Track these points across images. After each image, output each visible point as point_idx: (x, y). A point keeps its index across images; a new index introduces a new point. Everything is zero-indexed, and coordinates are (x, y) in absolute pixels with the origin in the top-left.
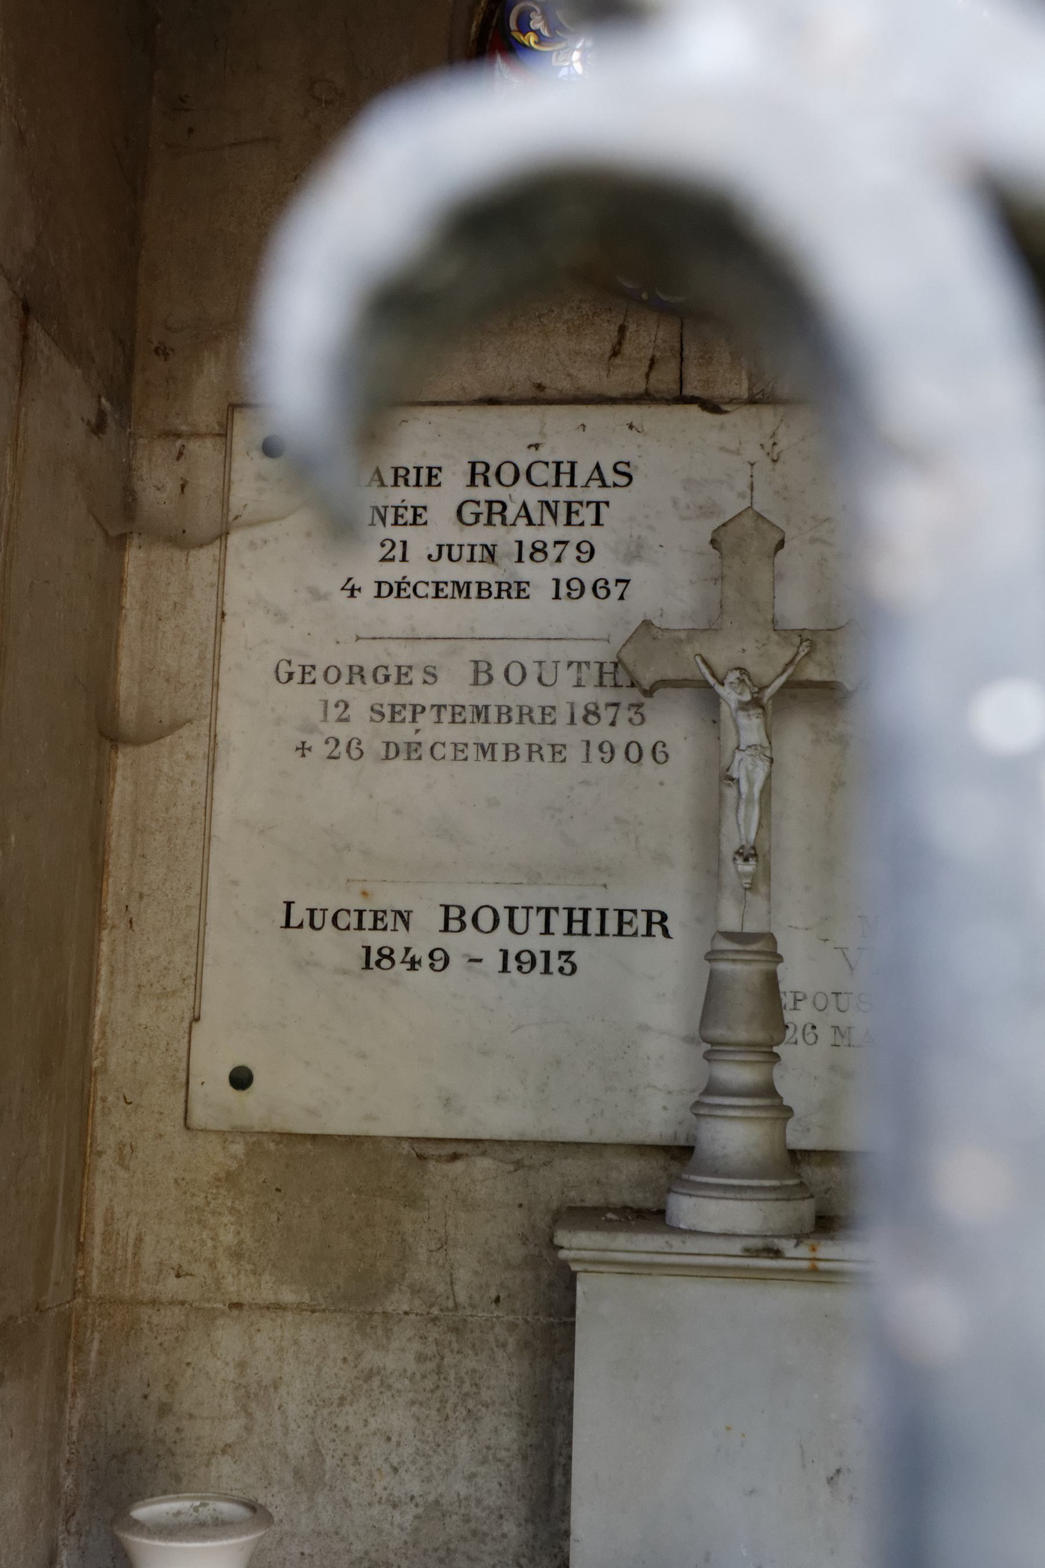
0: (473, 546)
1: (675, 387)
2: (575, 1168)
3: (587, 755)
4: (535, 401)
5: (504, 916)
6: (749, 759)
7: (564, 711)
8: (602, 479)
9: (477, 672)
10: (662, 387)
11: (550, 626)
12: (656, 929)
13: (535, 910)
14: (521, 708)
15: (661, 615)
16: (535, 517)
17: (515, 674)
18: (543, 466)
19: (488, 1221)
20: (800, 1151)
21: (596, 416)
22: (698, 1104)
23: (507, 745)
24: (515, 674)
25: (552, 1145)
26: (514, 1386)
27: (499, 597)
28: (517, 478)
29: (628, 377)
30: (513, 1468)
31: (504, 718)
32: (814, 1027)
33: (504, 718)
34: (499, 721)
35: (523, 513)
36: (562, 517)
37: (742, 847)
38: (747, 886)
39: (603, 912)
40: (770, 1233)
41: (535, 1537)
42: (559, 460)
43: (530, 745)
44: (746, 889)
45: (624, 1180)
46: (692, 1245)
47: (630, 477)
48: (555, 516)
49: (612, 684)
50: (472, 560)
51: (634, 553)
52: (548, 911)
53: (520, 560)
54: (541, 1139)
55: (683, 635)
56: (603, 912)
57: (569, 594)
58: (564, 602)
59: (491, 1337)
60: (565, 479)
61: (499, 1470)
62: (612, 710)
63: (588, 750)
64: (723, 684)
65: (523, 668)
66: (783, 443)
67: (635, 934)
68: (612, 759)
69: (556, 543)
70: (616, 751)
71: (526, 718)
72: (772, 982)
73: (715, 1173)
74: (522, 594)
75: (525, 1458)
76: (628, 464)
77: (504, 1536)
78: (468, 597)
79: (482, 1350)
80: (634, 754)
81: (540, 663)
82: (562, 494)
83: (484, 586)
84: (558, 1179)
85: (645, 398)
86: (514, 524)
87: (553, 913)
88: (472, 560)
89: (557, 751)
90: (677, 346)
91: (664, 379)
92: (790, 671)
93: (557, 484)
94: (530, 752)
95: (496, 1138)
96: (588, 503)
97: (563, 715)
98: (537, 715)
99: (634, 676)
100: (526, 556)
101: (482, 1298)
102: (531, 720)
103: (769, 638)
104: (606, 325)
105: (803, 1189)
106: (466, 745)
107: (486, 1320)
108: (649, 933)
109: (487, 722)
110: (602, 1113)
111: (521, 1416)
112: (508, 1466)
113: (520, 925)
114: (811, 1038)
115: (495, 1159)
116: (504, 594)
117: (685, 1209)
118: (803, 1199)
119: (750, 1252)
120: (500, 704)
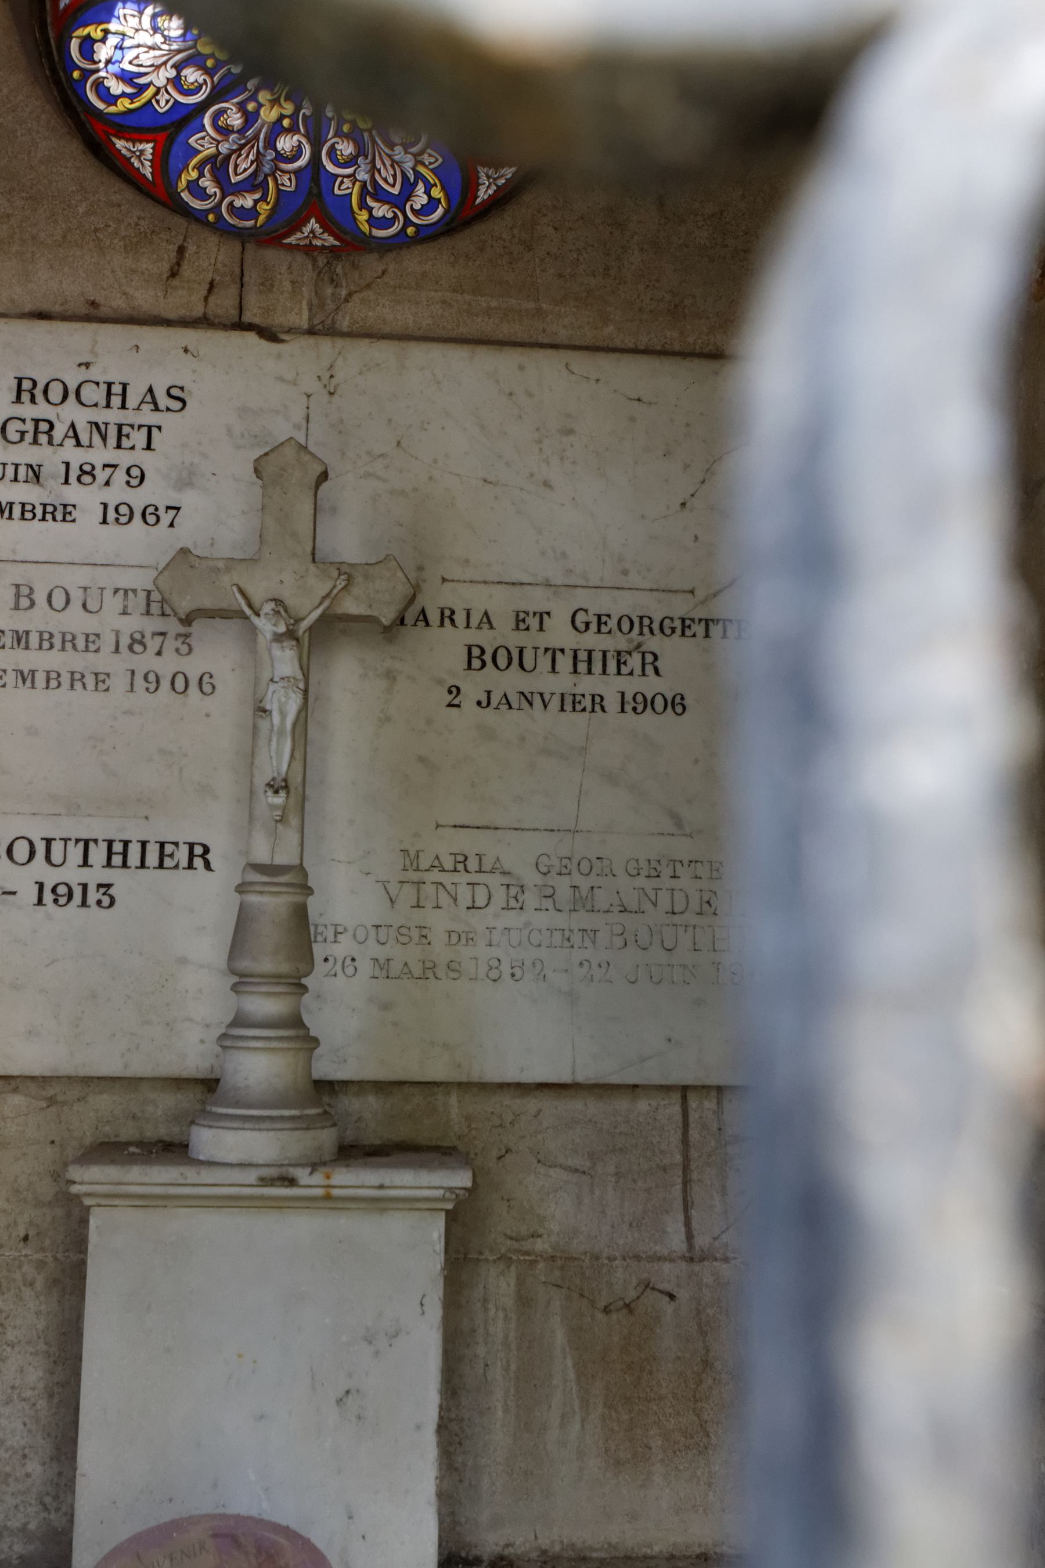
0: (17, 466)
1: (235, 313)
2: (104, 1102)
3: (132, 684)
4: (87, 319)
5: (40, 848)
6: (282, 690)
7: (108, 639)
8: (155, 403)
9: (18, 596)
10: (220, 312)
11: (94, 551)
12: (198, 862)
13: (73, 841)
14: (64, 634)
15: (212, 544)
16: (84, 438)
17: (59, 600)
18: (94, 386)
19: (17, 1159)
20: (338, 1082)
21: (151, 337)
22: (224, 1036)
23: (48, 672)
24: (59, 600)
25: (87, 1081)
26: (41, 1324)
27: (44, 519)
28: (65, 397)
29: (186, 299)
30: (38, 1407)
31: (46, 645)
32: (353, 960)
33: (46, 645)
34: (40, 648)
35: (71, 433)
36: (112, 441)
37: (274, 779)
38: (278, 818)
39: (144, 844)
40: (287, 1162)
41: (60, 1474)
42: (110, 380)
43: (72, 673)
44: (277, 821)
45: (158, 1113)
46: (207, 1175)
47: (184, 402)
48: (104, 439)
49: (160, 613)
50: (16, 480)
51: (186, 480)
52: (87, 843)
53: (66, 482)
54: (73, 1074)
55: (221, 564)
56: (144, 844)
57: (117, 520)
58: (112, 528)
59: (18, 1276)
60: (116, 401)
61: (23, 1409)
62: (159, 639)
63: (132, 679)
64: (258, 615)
65: (67, 594)
66: (340, 376)
67: (176, 867)
68: (157, 689)
69: (105, 466)
70: (162, 681)
71: (69, 645)
72: (300, 915)
73: (237, 1104)
74: (68, 518)
75: (51, 1396)
76: (182, 388)
77: (28, 1475)
78: (10, 518)
79: (9, 1290)
80: (181, 685)
81: (85, 589)
82: (113, 416)
83: (28, 507)
84: (91, 1114)
85: (204, 322)
86: (61, 445)
87: (92, 845)
88: (16, 480)
89: (101, 679)
90: (237, 271)
91: (224, 303)
92: (326, 603)
93: (108, 406)
94: (73, 680)
95: (27, 1073)
96: (140, 427)
97: (107, 642)
98: (81, 643)
99: (186, 605)
100: (73, 478)
101: (10, 1237)
102: (74, 647)
103: (307, 570)
104: (164, 244)
105: (327, 1118)
106: (583, 696)
107: (15, 1259)
108: (190, 866)
109: (27, 648)
110: (138, 1048)
111: (48, 1354)
112: (34, 1405)
113: (57, 856)
114: (350, 971)
115: (26, 1095)
116: (49, 517)
117: (207, 1140)
118: (323, 1128)
119: (264, 1182)
120: (42, 629)
